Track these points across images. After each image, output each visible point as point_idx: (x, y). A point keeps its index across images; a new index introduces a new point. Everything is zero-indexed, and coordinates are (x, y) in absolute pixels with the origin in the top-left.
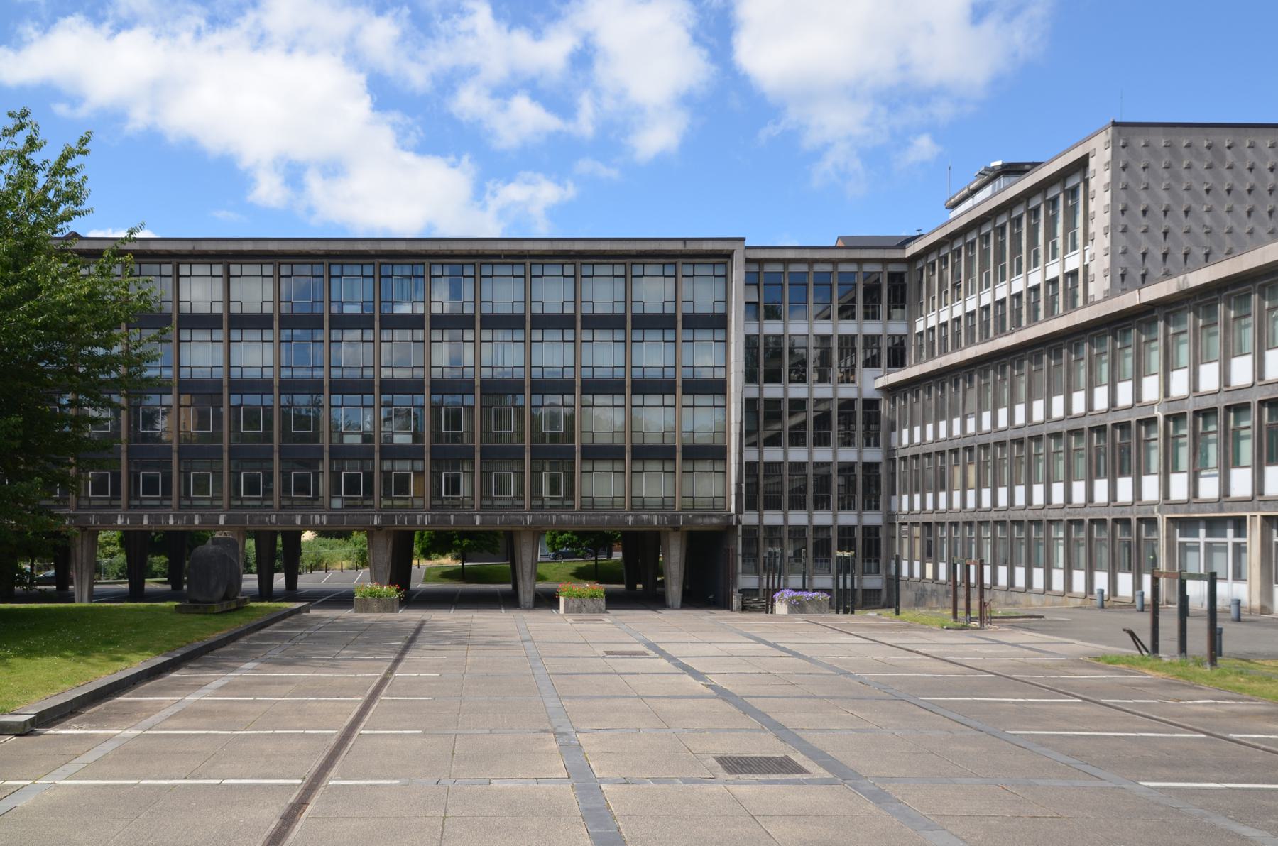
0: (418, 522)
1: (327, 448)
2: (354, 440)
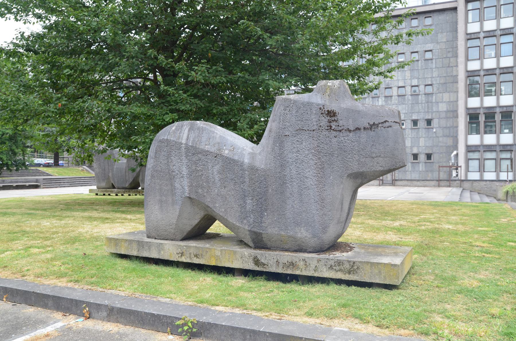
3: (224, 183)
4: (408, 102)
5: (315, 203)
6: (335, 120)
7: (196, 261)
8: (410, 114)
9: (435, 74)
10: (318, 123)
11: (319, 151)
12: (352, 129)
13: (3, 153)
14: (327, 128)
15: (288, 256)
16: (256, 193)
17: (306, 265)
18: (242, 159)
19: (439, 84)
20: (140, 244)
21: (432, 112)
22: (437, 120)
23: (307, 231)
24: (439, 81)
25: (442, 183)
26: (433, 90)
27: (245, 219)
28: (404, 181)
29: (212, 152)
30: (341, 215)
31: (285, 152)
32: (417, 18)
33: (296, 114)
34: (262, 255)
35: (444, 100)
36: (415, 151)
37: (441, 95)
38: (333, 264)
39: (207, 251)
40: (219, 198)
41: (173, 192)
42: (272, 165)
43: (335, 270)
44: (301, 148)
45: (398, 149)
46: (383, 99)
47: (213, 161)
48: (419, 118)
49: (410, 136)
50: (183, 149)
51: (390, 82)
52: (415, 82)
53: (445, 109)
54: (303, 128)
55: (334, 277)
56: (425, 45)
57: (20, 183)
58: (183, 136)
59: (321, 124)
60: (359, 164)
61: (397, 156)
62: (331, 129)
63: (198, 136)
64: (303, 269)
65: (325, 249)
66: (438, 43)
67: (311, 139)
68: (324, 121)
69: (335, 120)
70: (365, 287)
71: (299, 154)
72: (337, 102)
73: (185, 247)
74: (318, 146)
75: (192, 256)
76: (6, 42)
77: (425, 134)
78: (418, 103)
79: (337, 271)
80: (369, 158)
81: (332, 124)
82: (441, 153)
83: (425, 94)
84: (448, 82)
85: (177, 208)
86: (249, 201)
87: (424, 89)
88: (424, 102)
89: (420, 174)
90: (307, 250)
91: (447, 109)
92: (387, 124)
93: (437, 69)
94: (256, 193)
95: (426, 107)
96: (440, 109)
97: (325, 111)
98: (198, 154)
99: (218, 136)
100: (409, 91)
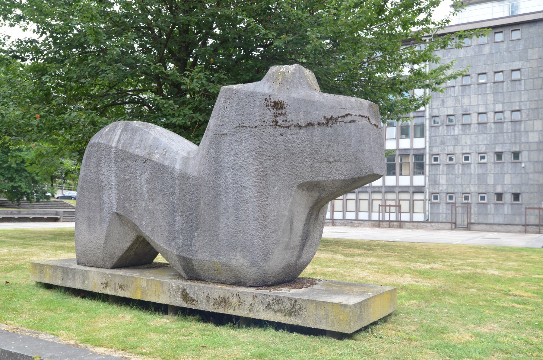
3: (152, 195)
4: (490, 131)
5: (254, 221)
6: (282, 113)
7: (121, 294)
8: (493, 146)
9: (524, 98)
10: (261, 118)
11: (261, 153)
12: (303, 125)
13: (22, 181)
14: (271, 124)
15: (219, 289)
16: (186, 207)
17: (240, 302)
18: (172, 165)
19: (529, 109)
20: (65, 271)
21: (520, 144)
22: (527, 152)
23: (244, 258)
24: (530, 106)
25: (529, 229)
26: (522, 117)
27: (173, 240)
28: (481, 225)
29: (141, 157)
30: (290, 239)
31: (222, 156)
32: (502, 32)
33: (236, 107)
34: (191, 287)
35: (536, 129)
36: (499, 190)
37: (531, 122)
38: (271, 302)
39: (132, 281)
40: (146, 214)
41: (101, 208)
42: (206, 172)
43: (274, 310)
44: (240, 150)
45: (363, 151)
46: (460, 127)
47: (142, 168)
48: (504, 150)
49: (493, 172)
50: (113, 153)
51: (468, 107)
52: (499, 108)
53: (536, 140)
54: (244, 125)
55: (272, 320)
56: (511, 63)
57: (38, 215)
58: (114, 138)
59: (265, 119)
60: (312, 171)
61: (362, 161)
62: (276, 125)
63: (130, 138)
64: (236, 308)
65: (270, 283)
66: (527, 60)
67: (253, 138)
68: (269, 115)
69: (282, 113)
70: (310, 335)
71: (236, 157)
72: (288, 90)
73: (110, 276)
74: (260, 147)
75: (117, 287)
77: (511, 169)
78: (502, 132)
79: (276, 312)
80: (325, 163)
81: (278, 119)
82: (532, 193)
83: (512, 122)
84: (540, 107)
85: (105, 226)
86: (178, 218)
87: (510, 116)
88: (510, 131)
89: (505, 218)
90: (246, 283)
91: (539, 139)
92: (349, 118)
93: (527, 91)
94: (186, 207)
95: (513, 137)
96: (531, 140)
97: (271, 102)
98: (127, 159)
99: (151, 138)
100: (492, 117)
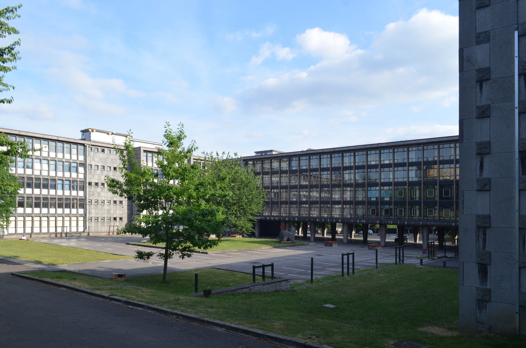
0: (389, 223)
1: (379, 202)
2: (374, 199)
36: (115, 216)
46: (100, 188)
48: (117, 200)
49: (113, 208)
76: (135, 252)
